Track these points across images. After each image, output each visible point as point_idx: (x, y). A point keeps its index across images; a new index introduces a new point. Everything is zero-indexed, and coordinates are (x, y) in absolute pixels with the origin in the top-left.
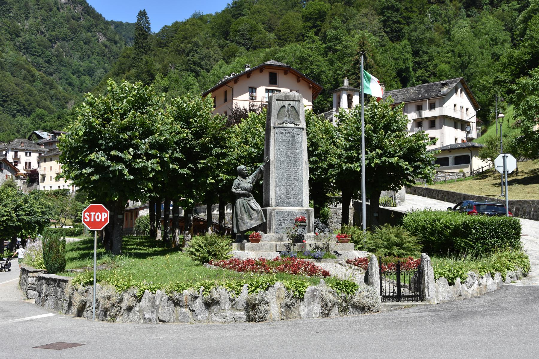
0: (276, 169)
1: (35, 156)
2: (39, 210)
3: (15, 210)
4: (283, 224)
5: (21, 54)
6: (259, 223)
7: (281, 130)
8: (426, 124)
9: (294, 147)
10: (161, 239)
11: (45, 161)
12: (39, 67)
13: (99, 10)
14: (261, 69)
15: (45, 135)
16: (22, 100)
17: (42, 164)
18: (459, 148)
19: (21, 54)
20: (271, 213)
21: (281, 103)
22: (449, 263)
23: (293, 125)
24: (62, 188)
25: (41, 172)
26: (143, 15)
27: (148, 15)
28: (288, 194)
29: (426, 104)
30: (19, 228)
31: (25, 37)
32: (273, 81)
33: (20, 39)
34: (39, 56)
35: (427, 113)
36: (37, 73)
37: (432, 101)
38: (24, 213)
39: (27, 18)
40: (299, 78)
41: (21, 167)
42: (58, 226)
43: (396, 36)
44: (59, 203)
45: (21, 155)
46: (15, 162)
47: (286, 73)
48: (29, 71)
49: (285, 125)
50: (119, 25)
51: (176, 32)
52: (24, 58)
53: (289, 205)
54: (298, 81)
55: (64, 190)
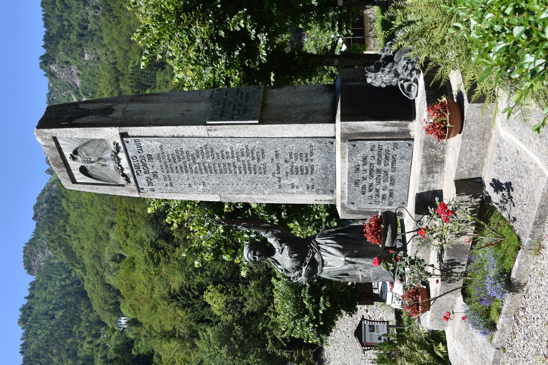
0: (240, 192)
4: (382, 192)
9: (178, 156)
10: (291, 225)
20: (352, 212)
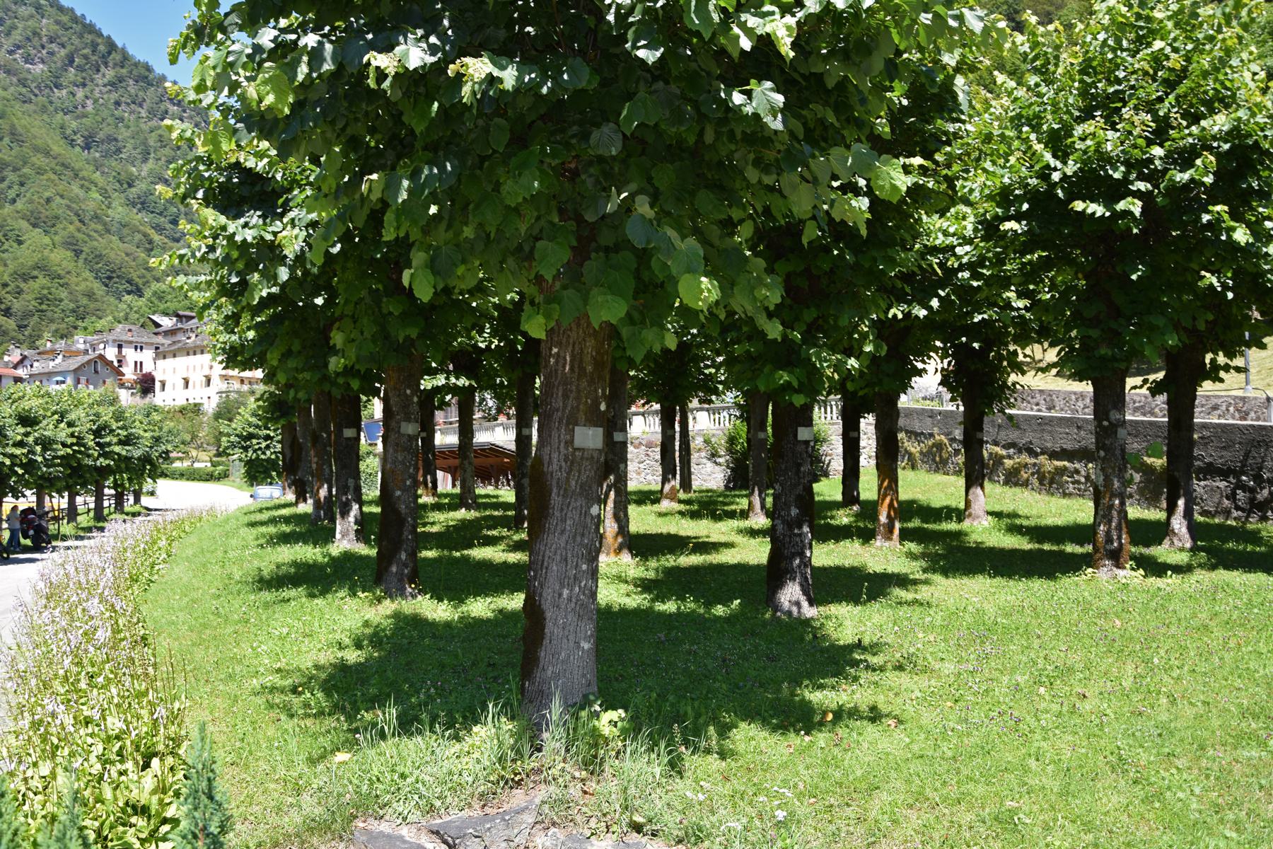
2: (148, 435)
3: (97, 433)
5: (135, 211)
11: (164, 358)
12: (159, 229)
15: (167, 322)
16: (134, 276)
17: (160, 363)
19: (135, 211)
24: (191, 401)
25: (158, 377)
30: (104, 472)
33: (133, 190)
34: (161, 214)
36: (156, 238)
38: (115, 440)
39: (145, 160)
42: (186, 464)
44: (188, 424)
46: (119, 361)
48: (145, 235)
52: (140, 218)
55: (195, 405)
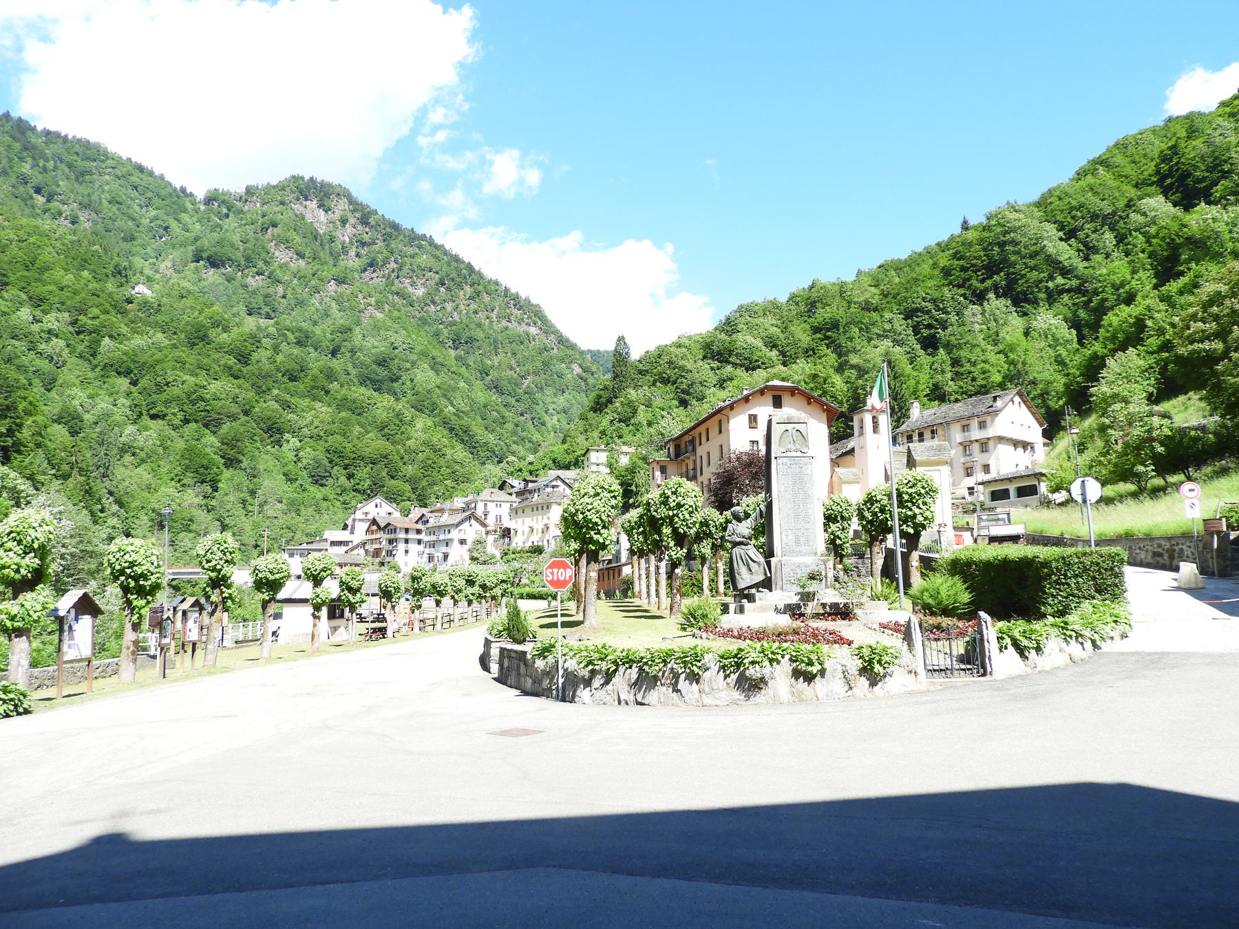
1: (506, 508)
6: (761, 578)
7: (785, 460)
8: (976, 448)
13: (573, 339)
14: (762, 392)
18: (1022, 477)
21: (784, 427)
22: (1018, 627)
23: (799, 454)
26: (621, 339)
27: (627, 341)
28: (797, 541)
29: (974, 423)
31: (494, 374)
32: (777, 403)
35: (976, 434)
37: (981, 419)
40: (809, 399)
41: (491, 521)
43: (930, 344)
45: (491, 506)
47: (793, 394)
49: (789, 454)
50: (596, 355)
51: (660, 356)
53: (800, 553)
54: (809, 403)
